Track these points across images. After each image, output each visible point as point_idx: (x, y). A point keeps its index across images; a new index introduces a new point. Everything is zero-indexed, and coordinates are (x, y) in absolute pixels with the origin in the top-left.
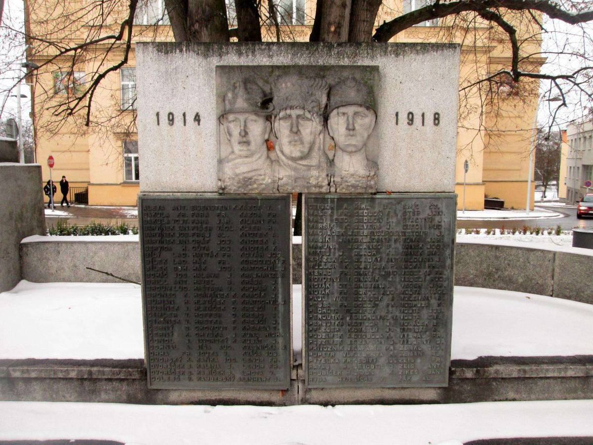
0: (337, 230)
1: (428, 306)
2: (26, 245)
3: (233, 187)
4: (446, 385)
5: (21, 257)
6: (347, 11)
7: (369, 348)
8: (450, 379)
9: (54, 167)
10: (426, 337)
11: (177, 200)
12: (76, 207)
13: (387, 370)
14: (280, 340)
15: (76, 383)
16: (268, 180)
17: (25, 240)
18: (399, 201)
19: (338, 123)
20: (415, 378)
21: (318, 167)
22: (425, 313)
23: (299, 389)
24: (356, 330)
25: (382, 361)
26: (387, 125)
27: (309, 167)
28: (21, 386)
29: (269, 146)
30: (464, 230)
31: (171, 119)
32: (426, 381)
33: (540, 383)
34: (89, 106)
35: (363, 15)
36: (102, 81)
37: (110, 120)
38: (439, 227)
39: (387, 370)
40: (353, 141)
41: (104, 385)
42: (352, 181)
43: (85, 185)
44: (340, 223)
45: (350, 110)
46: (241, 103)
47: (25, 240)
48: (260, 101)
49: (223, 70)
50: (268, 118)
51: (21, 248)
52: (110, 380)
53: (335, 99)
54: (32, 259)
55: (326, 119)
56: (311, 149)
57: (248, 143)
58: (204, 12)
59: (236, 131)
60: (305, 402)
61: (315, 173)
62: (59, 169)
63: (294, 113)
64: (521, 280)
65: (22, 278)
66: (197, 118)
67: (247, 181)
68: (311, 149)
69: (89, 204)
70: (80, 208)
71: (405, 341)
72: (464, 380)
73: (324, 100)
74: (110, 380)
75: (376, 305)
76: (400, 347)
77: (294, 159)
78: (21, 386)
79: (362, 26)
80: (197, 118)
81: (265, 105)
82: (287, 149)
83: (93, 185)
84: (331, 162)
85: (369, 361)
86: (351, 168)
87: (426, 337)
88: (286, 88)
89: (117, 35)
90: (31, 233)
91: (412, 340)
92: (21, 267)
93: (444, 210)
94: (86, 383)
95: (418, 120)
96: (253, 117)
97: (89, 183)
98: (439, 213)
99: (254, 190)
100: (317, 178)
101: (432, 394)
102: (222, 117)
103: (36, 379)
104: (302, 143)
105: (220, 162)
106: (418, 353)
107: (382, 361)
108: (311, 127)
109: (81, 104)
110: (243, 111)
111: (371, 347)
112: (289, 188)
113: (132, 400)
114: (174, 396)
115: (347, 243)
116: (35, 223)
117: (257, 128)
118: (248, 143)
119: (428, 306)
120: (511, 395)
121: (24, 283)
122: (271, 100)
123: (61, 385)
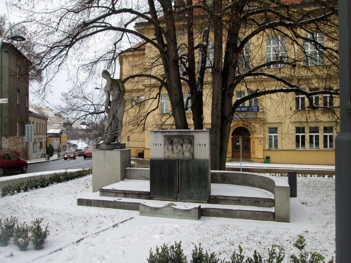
0: (186, 166)
1: (204, 182)
2: (127, 170)
3: (166, 158)
4: (208, 199)
5: (125, 173)
6: (220, 101)
7: (192, 191)
8: (209, 199)
9: (130, 140)
10: (203, 189)
11: (157, 160)
12: (138, 160)
13: (196, 196)
14: (175, 188)
15: (137, 195)
16: (172, 156)
17: (126, 168)
18: (197, 161)
19: (184, 146)
20: (202, 198)
21: (181, 154)
22: (203, 184)
23: (179, 198)
24: (190, 187)
25: (195, 193)
26: (195, 146)
27: (179, 154)
28: (127, 195)
29: (173, 150)
30: (309, 175)
31: (156, 145)
32: (204, 198)
33: (229, 201)
34: (144, 124)
35: (227, 100)
36: (149, 115)
37: (152, 126)
38: (205, 166)
39: (196, 196)
40: (187, 150)
41: (143, 196)
42: (187, 157)
43: (143, 149)
44: (186, 165)
45: (186, 144)
46: (167, 143)
47: (126, 168)
48: (170, 142)
49: (165, 136)
50: (172, 145)
51: (126, 170)
52: (143, 195)
53: (184, 142)
54: (128, 173)
55: (182, 146)
56: (180, 151)
57: (168, 150)
58: (176, 103)
59: (166, 148)
60: (180, 201)
61: (180, 155)
62: (132, 141)
63: (177, 144)
64: (251, 183)
65: (125, 178)
66: (161, 145)
67: (169, 157)
68: (180, 151)
69: (144, 158)
70: (140, 160)
71: (199, 190)
72: (212, 199)
73: (182, 142)
74: (143, 195)
75: (193, 182)
76: (198, 191)
77: (177, 153)
78: (127, 195)
79: (227, 104)
80: (161, 145)
81: (171, 143)
82: (175, 151)
83: (147, 149)
84: (184, 153)
85: (192, 193)
86: (187, 155)
87: (203, 189)
88: (175, 140)
89: (155, 97)
90: (128, 167)
91: (201, 190)
92: (125, 175)
93: (206, 163)
94: (139, 195)
95: (201, 145)
96: (169, 145)
97: (145, 149)
98: (205, 163)
99: (170, 158)
100: (181, 156)
101: (206, 202)
102: (164, 145)
103: (130, 194)
104: (178, 150)
105: (164, 153)
106: (202, 192)
107: (195, 193)
108: (179, 147)
109: (142, 123)
110: (167, 144)
111: (193, 190)
112: (176, 158)
113: (147, 199)
114: (155, 198)
115: (188, 169)
116: (129, 165)
117: (170, 147)
118: (168, 150)
119: (204, 182)
120: (223, 203)
121: (125, 179)
122: (172, 142)
123: (134, 195)
